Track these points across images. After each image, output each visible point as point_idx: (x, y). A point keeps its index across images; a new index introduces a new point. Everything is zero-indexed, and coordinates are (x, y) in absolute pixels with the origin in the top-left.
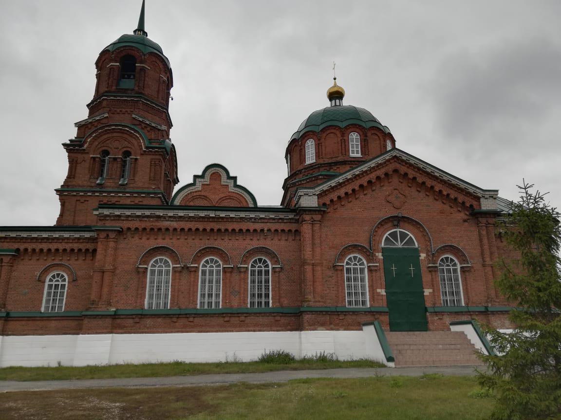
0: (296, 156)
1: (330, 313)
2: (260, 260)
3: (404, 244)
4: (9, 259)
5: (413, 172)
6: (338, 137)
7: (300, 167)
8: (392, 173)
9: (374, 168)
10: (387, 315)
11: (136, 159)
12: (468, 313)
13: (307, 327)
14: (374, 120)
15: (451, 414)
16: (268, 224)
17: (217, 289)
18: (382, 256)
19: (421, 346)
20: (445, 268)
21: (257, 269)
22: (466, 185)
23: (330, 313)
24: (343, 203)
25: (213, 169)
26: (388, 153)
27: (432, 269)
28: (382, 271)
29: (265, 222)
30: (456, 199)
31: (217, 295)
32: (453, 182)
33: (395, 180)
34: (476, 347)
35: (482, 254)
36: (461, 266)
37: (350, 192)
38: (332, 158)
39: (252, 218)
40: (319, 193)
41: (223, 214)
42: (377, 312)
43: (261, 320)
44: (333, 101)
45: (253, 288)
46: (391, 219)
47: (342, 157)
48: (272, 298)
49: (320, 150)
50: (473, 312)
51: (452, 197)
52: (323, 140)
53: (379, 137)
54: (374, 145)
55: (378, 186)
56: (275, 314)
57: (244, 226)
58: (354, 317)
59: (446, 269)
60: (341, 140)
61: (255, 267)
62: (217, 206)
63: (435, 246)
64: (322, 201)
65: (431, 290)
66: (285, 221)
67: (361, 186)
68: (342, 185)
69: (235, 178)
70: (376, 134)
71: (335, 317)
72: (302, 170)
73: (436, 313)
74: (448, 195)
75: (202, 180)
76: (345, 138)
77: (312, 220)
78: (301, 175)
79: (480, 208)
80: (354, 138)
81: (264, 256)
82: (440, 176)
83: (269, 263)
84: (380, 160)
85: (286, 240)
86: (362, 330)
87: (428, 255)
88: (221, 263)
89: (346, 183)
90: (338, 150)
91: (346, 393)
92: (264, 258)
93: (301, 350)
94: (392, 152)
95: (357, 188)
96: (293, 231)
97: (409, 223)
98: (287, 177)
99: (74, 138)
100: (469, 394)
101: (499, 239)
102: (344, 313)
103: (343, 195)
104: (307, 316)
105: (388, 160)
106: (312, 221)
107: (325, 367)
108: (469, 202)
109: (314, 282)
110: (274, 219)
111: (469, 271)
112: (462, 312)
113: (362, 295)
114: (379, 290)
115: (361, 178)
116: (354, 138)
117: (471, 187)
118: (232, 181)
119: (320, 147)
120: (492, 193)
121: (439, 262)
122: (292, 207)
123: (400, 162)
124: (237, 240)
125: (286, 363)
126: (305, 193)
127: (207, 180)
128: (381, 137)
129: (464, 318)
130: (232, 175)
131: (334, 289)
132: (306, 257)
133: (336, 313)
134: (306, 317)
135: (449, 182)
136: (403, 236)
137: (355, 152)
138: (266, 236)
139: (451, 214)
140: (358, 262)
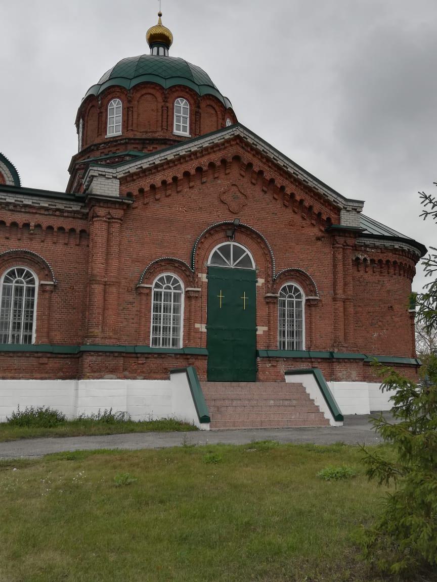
0: (93, 123)
1: (124, 355)
2: (21, 272)
3: (238, 263)
5: (261, 164)
6: (157, 101)
7: (97, 141)
8: (231, 160)
9: (206, 149)
10: (205, 359)
12: (310, 359)
13: (88, 374)
14: (213, 87)
15: (300, 513)
16: (37, 216)
18: (207, 278)
19: (247, 402)
20: (287, 299)
21: (13, 285)
22: (326, 190)
23: (124, 355)
24: (157, 197)
26: (228, 130)
27: (270, 300)
28: (205, 298)
29: (33, 213)
30: (311, 207)
32: (310, 184)
33: (235, 171)
34: (316, 404)
35: (335, 284)
36: (307, 298)
37: (170, 180)
38: (146, 132)
39: (10, 203)
40: (123, 175)
42: (192, 355)
43: (16, 362)
44: (155, 49)
46: (224, 227)
47: (161, 133)
48: (37, 331)
49: (130, 118)
50: (314, 358)
51: (306, 204)
52: (136, 103)
53: (216, 111)
54: (208, 122)
55: (211, 177)
56: (40, 355)
58: (159, 361)
59: (288, 300)
60: (162, 107)
61: (12, 282)
63: (278, 270)
64: (126, 190)
65: (266, 328)
66: (66, 214)
67: (187, 174)
68: (159, 169)
70: (214, 108)
71: (132, 361)
72: (101, 144)
73: (269, 358)
74: (302, 201)
76: (168, 104)
77: (109, 216)
78: (98, 153)
79: (339, 223)
80: (182, 106)
81: (27, 265)
82: (294, 173)
83: (35, 276)
84: (216, 138)
85: (66, 244)
86: (169, 379)
87: (267, 281)
89: (165, 167)
90: (157, 121)
91: (134, 477)
92: (27, 269)
93: (76, 407)
94: (234, 129)
95: (180, 176)
97: (247, 235)
98: (77, 152)
100: (322, 473)
101: (356, 268)
102: (146, 355)
103: (159, 184)
104: (90, 358)
105: (228, 141)
106: (109, 219)
107: (109, 431)
108: (326, 213)
109: (105, 309)
111: (315, 305)
112: (301, 358)
113: (173, 331)
114: (197, 326)
115: (187, 161)
116: (182, 106)
117: (331, 193)
119: (130, 113)
120: (356, 205)
121: (280, 291)
122: (81, 194)
123: (244, 146)
125: (50, 427)
126: (100, 173)
128: (219, 113)
129: (304, 366)
131: (135, 321)
132: (95, 272)
133: (134, 355)
134: (88, 360)
135: (304, 183)
136: (238, 252)
137: (181, 127)
138: (32, 234)
139: (303, 227)
140: (172, 285)
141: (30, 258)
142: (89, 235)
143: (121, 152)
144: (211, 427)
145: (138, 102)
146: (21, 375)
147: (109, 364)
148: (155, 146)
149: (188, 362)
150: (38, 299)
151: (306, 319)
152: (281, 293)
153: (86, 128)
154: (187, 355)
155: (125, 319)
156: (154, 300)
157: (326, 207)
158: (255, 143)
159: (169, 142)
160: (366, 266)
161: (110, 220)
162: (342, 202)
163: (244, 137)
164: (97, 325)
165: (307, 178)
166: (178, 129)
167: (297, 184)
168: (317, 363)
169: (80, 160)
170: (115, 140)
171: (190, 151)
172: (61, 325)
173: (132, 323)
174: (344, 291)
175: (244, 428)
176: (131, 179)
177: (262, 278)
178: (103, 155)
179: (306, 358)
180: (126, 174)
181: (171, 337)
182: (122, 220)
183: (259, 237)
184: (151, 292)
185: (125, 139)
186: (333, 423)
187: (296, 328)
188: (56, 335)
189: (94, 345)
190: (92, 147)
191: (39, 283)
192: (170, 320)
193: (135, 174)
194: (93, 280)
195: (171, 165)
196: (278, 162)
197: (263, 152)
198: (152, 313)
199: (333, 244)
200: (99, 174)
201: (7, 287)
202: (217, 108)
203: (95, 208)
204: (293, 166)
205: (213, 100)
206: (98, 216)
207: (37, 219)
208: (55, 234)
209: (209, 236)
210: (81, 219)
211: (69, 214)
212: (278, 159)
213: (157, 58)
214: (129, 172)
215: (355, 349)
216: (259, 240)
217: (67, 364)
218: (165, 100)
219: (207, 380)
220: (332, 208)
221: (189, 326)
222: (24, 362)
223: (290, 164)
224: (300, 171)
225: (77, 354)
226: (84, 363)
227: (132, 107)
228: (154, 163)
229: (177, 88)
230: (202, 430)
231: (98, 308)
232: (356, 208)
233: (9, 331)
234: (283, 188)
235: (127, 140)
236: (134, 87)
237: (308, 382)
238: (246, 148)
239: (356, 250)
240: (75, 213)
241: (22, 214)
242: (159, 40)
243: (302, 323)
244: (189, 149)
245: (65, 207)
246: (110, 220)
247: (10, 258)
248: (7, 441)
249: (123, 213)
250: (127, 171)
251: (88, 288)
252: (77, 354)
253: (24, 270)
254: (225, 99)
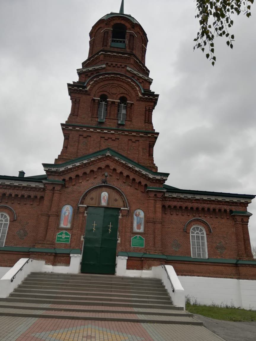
4: (161, 195)
11: (132, 104)
99: (76, 82)
163: (148, 79)
187: (198, 251)
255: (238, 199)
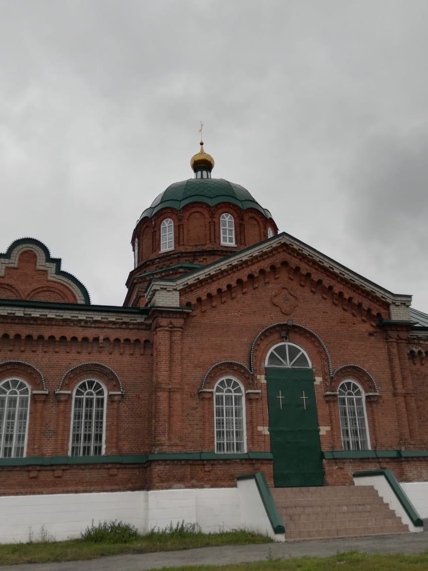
0: (147, 241)
1: (191, 462)
2: (91, 384)
5: (308, 268)
8: (280, 266)
9: (256, 257)
10: (270, 464)
12: (377, 459)
13: (157, 485)
14: (254, 201)
16: (105, 330)
17: (20, 428)
18: (266, 379)
19: (319, 509)
20: (346, 397)
21: (84, 397)
22: (373, 287)
23: (191, 462)
25: (24, 246)
28: (265, 400)
29: (102, 328)
31: (21, 438)
32: (357, 282)
33: (284, 276)
34: (391, 508)
35: (393, 379)
36: (367, 395)
37: (224, 288)
39: (81, 320)
40: (182, 287)
41: (36, 313)
42: (257, 460)
43: (88, 474)
44: (199, 173)
45: (77, 427)
46: (278, 329)
48: (106, 441)
50: (382, 458)
51: (355, 301)
52: (186, 221)
53: (258, 222)
54: (252, 232)
56: (110, 466)
57: (69, 332)
60: (210, 222)
61: (83, 394)
62: (28, 299)
63: (335, 367)
64: (185, 300)
65: (328, 428)
66: (131, 327)
69: (58, 261)
70: (256, 220)
71: (198, 468)
72: (156, 259)
73: (335, 460)
74: (350, 299)
75: (7, 261)
76: (214, 220)
77: (170, 326)
78: (154, 267)
80: (227, 221)
82: (340, 273)
83: (104, 387)
86: (235, 486)
87: (325, 379)
88: (29, 387)
90: (206, 235)
92: (96, 381)
93: (146, 520)
95: (234, 284)
96: (142, 342)
97: (301, 335)
103: (215, 293)
104: (159, 467)
105: (275, 249)
106: (171, 328)
109: (170, 416)
110: (114, 323)
112: (368, 458)
113: (237, 435)
114: (260, 428)
115: (239, 270)
117: (378, 290)
118: (54, 266)
119: (181, 230)
121: (339, 388)
122: (142, 305)
123: (290, 252)
124: (57, 352)
125: (125, 542)
126: (162, 287)
127: (14, 261)
128: (260, 223)
129: (372, 467)
130: (53, 255)
132: (160, 380)
134: (157, 469)
135: (350, 281)
136: (294, 352)
137: (227, 239)
138: (101, 347)
139: (354, 324)
140: (233, 388)
141: (99, 370)
142: (152, 345)
143: (175, 265)
144: (286, 537)
145: (188, 219)
146: (92, 488)
147: (177, 473)
148: (205, 257)
149: (380, 465)
150: (107, 409)
151: (368, 416)
152: (339, 391)
153: (141, 246)
154: (252, 460)
155: (190, 425)
156: (216, 405)
157: (375, 303)
158: (301, 249)
159: (217, 253)
160: (422, 359)
161: (172, 330)
162: (391, 297)
163: (290, 244)
164: (164, 433)
165: (353, 277)
166: (225, 240)
167: (344, 283)
168: (385, 463)
169: (137, 274)
170: (168, 255)
171: (242, 260)
172: (128, 434)
173: (197, 429)
174: (404, 386)
175: (320, 538)
176: (190, 290)
177: (319, 376)
178: (157, 269)
179: (373, 458)
180: (186, 286)
181: (235, 442)
182: (182, 328)
183: (312, 335)
184: (213, 397)
185: (178, 253)
186: (412, 528)
188: (124, 445)
189: (162, 453)
190: (148, 263)
191: (108, 394)
192: (233, 424)
193: (193, 285)
194: (159, 388)
195: (225, 274)
196: (324, 264)
197: (309, 257)
198: (215, 418)
199: (387, 339)
200: (161, 288)
201: (89, 400)
202: (259, 219)
203: (158, 318)
204: (338, 267)
205: (255, 213)
206: (161, 327)
207: (105, 333)
208: (122, 345)
209: (264, 338)
210: (145, 329)
211: (135, 326)
212: (323, 262)
213: (202, 181)
214: (187, 284)
215: (423, 446)
216: (313, 339)
217: (135, 474)
218: (212, 216)
219: (274, 486)
220: (380, 303)
221: (252, 429)
222: (95, 474)
223: (336, 266)
224: (345, 271)
225: (145, 463)
226: (152, 472)
227: (183, 225)
228: (210, 274)
229: (222, 205)
230: (277, 542)
231: (164, 415)
232: (404, 302)
233: (80, 443)
234: (331, 288)
235: (179, 254)
236: (184, 208)
237: (380, 484)
238: (292, 253)
239: (409, 343)
240: (139, 325)
241: (93, 329)
242: (203, 165)
243: (364, 421)
244: (241, 259)
245: (131, 320)
246: (172, 330)
247: (82, 371)
248: (89, 559)
249: (183, 322)
250: (186, 283)
251: (154, 396)
252: (145, 463)
253: (94, 382)
254: (266, 212)
255: (104, 315)
